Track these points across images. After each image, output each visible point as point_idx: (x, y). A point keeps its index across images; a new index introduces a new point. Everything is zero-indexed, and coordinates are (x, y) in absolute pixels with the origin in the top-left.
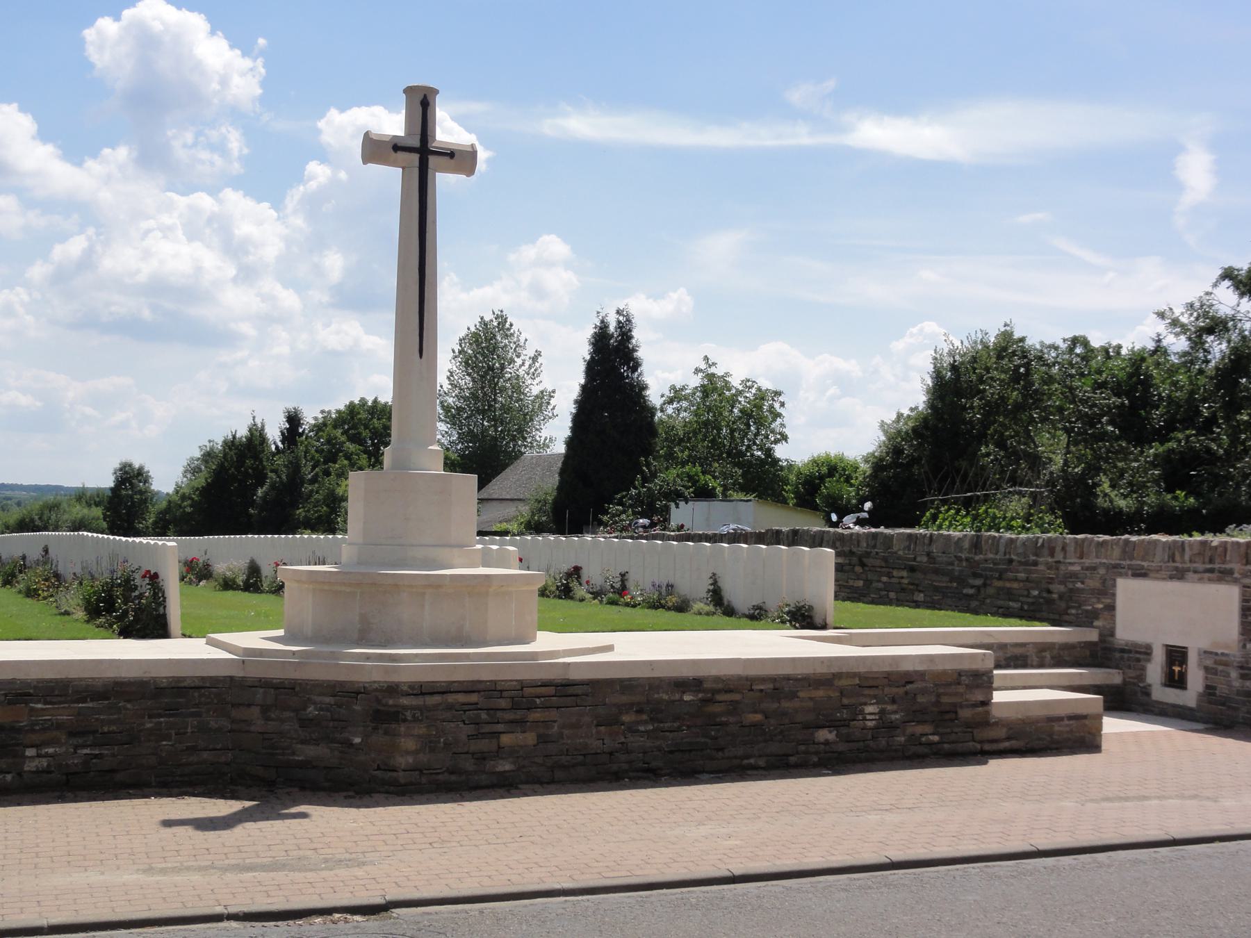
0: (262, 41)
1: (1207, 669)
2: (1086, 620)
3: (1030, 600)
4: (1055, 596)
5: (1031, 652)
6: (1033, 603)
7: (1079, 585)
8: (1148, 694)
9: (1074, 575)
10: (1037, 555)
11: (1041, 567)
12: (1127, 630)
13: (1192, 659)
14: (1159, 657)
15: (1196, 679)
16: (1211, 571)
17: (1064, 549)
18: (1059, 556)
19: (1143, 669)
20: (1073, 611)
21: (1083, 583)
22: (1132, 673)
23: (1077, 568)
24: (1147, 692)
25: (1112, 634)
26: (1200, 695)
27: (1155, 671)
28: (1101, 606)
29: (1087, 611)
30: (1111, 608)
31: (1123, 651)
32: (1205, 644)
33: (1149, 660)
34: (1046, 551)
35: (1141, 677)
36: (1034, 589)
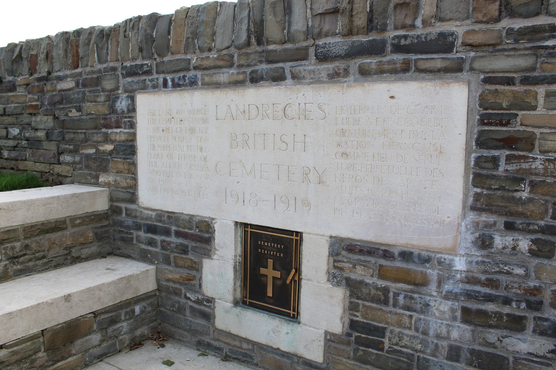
0: (282, 255)
1: (354, 287)
2: (92, 169)
3: (11, 143)
4: (41, 134)
5: (396, 252)
6: (15, 148)
7: (74, 113)
8: (209, 317)
9: (64, 98)
10: (12, 73)
11: (21, 91)
12: (155, 193)
13: (314, 262)
14: (227, 250)
15: (323, 307)
16: (375, 49)
17: (48, 56)
18: (43, 69)
19: (197, 267)
20: (67, 158)
21: (79, 109)
22: (173, 273)
23: (69, 84)
24: (205, 309)
25: (133, 198)
26: (331, 340)
27: (220, 275)
28: (109, 147)
29: (88, 156)
30: (128, 149)
31: (151, 229)
32: (356, 227)
33: (208, 254)
34: (25, 66)
35: (193, 280)
36: (13, 125)
